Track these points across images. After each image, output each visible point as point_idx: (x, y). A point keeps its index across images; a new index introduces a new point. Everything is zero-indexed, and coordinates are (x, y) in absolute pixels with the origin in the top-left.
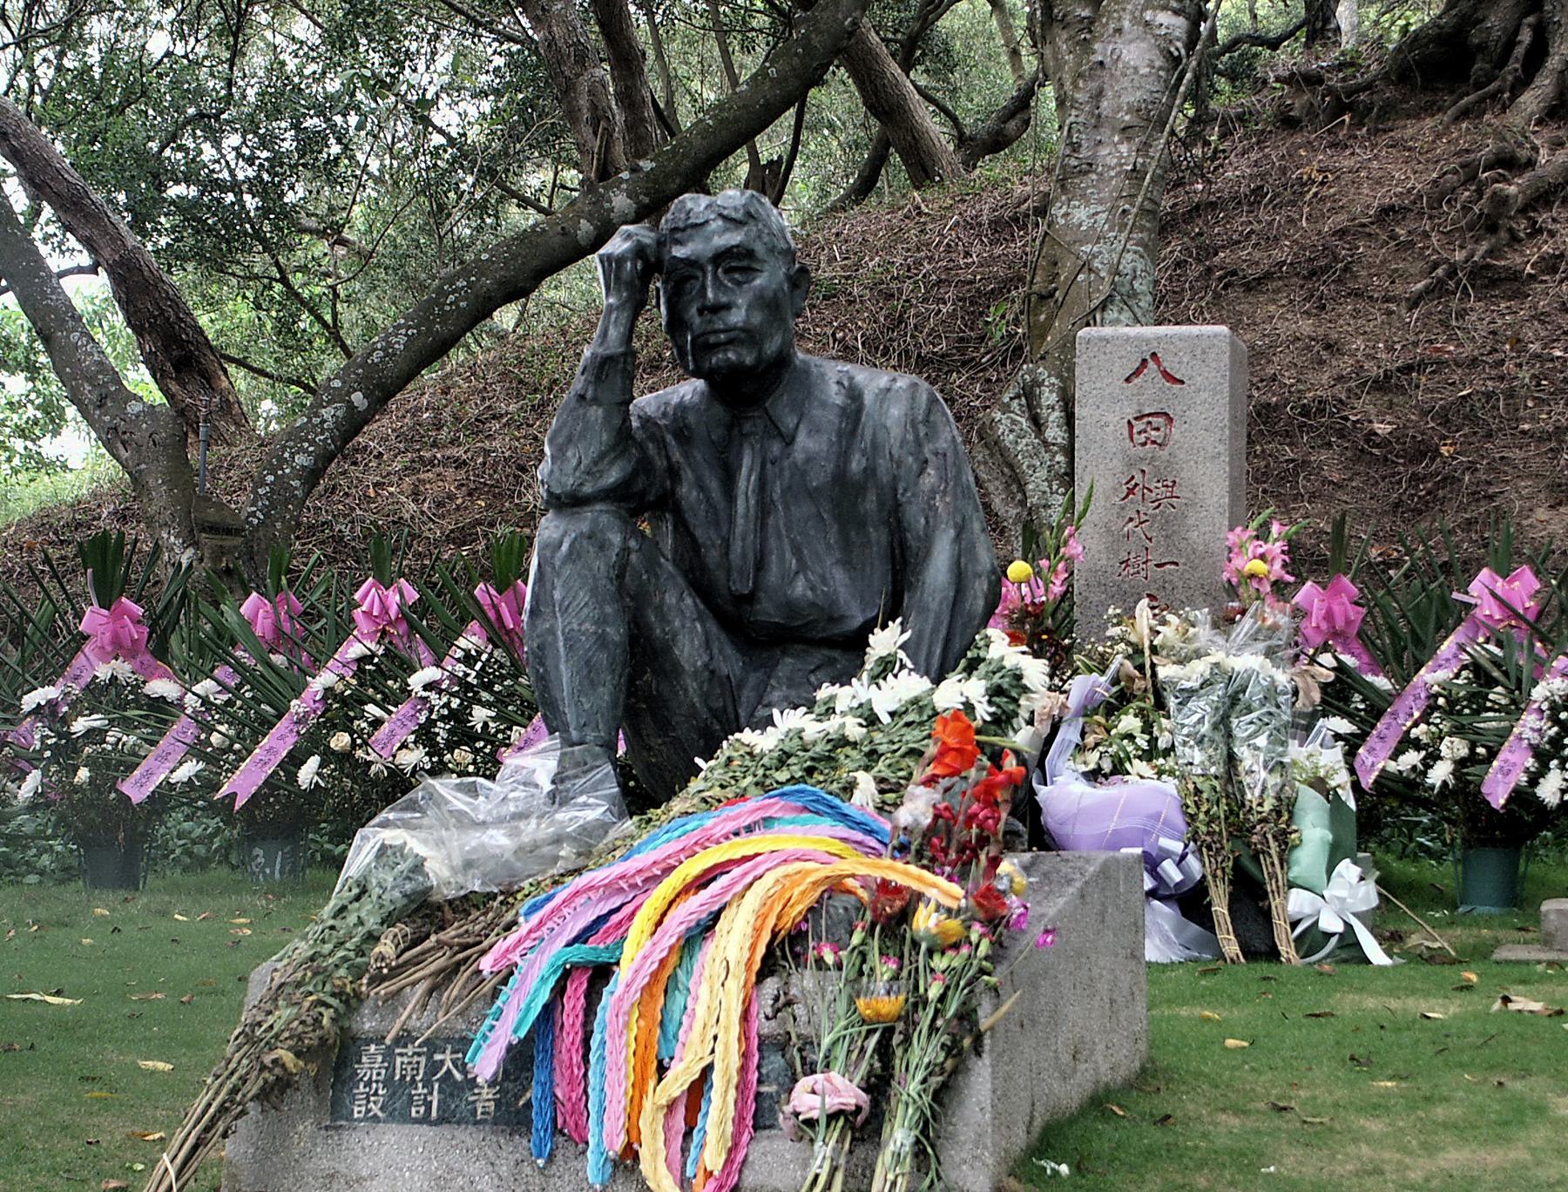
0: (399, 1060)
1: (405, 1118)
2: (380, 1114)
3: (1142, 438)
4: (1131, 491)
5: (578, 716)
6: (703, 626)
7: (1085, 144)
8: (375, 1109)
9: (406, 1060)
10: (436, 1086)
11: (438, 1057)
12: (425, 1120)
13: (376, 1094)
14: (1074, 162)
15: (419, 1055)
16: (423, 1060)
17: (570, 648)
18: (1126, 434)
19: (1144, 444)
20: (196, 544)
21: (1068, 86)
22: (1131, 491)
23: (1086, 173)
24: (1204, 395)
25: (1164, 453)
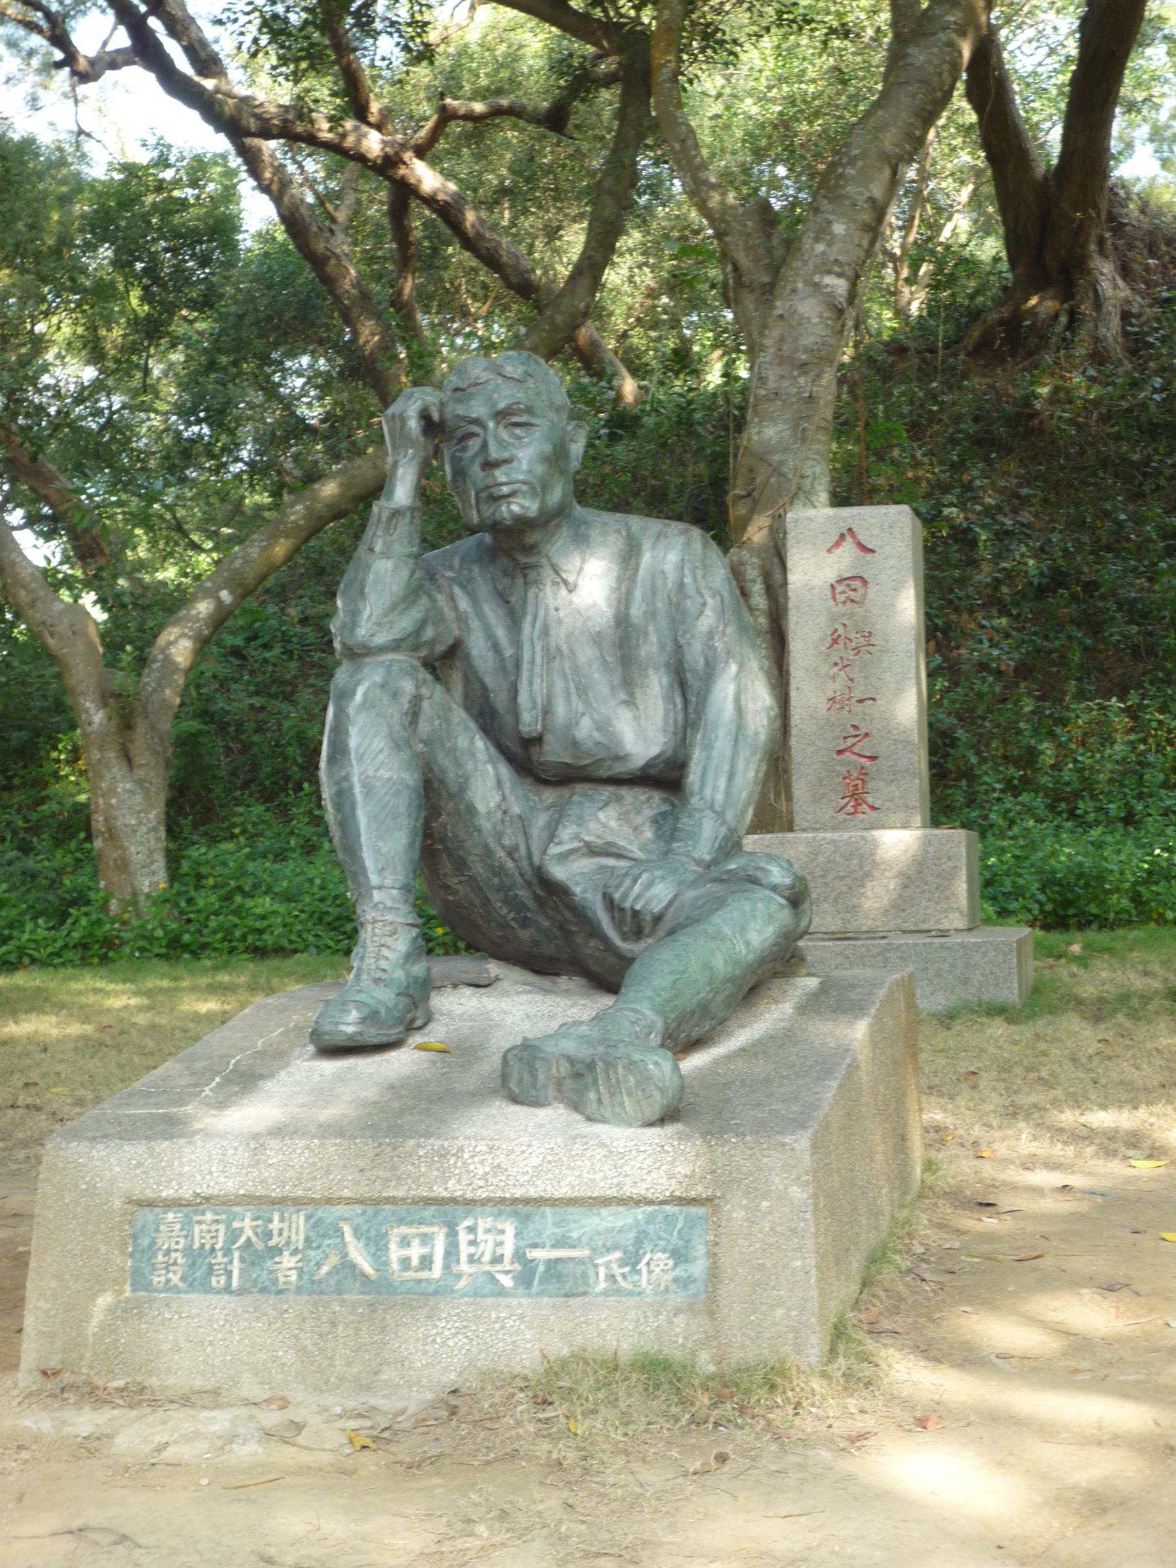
0: (197, 1229)
1: (207, 1289)
2: (181, 1284)
3: (842, 598)
4: (835, 642)
5: (376, 860)
6: (495, 768)
7: (771, 378)
8: (175, 1279)
9: (204, 1227)
10: (236, 1255)
11: (236, 1225)
12: (227, 1289)
13: (175, 1263)
14: (763, 392)
15: (217, 1221)
16: (222, 1227)
17: (367, 795)
18: (829, 594)
19: (844, 603)
20: (105, 705)
21: (755, 335)
22: (835, 642)
23: (773, 400)
24: (892, 562)
25: (860, 611)
